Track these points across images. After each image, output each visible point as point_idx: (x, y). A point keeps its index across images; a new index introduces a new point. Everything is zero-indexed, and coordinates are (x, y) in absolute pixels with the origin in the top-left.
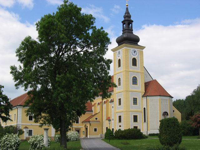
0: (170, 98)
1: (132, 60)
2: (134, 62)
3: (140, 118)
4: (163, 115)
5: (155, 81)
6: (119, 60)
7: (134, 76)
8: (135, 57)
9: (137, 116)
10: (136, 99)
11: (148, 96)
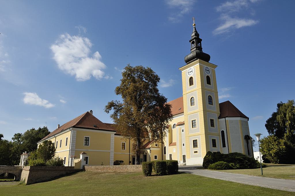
1: (206, 78)
3: (219, 143)
8: (209, 75)
11: (227, 117)
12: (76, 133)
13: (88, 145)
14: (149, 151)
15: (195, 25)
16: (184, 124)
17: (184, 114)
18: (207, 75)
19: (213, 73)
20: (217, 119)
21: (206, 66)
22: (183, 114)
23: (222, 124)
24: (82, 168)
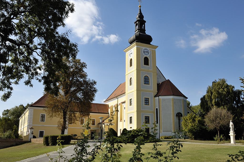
0: (185, 99)
1: (143, 59)
2: (146, 62)
3: (152, 120)
4: (177, 116)
5: (169, 80)
6: (131, 60)
7: (145, 75)
8: (147, 56)
9: (145, 64)
10: (148, 118)
11: (160, 96)
12: (33, 111)
13: (44, 121)
14: (104, 125)
15: (140, 7)
16: (125, 102)
17: (125, 95)
18: (145, 56)
19: (152, 54)
20: (154, 97)
21: (144, 48)
22: (125, 95)
23: (155, 102)
24: (29, 140)
